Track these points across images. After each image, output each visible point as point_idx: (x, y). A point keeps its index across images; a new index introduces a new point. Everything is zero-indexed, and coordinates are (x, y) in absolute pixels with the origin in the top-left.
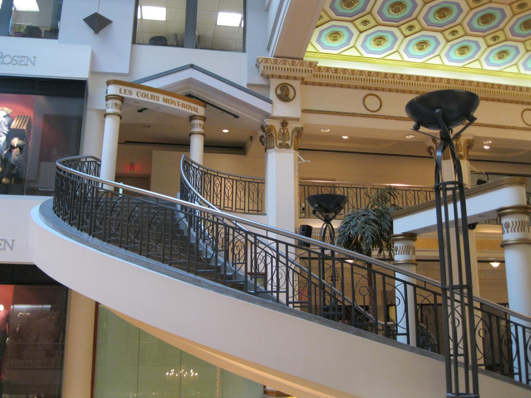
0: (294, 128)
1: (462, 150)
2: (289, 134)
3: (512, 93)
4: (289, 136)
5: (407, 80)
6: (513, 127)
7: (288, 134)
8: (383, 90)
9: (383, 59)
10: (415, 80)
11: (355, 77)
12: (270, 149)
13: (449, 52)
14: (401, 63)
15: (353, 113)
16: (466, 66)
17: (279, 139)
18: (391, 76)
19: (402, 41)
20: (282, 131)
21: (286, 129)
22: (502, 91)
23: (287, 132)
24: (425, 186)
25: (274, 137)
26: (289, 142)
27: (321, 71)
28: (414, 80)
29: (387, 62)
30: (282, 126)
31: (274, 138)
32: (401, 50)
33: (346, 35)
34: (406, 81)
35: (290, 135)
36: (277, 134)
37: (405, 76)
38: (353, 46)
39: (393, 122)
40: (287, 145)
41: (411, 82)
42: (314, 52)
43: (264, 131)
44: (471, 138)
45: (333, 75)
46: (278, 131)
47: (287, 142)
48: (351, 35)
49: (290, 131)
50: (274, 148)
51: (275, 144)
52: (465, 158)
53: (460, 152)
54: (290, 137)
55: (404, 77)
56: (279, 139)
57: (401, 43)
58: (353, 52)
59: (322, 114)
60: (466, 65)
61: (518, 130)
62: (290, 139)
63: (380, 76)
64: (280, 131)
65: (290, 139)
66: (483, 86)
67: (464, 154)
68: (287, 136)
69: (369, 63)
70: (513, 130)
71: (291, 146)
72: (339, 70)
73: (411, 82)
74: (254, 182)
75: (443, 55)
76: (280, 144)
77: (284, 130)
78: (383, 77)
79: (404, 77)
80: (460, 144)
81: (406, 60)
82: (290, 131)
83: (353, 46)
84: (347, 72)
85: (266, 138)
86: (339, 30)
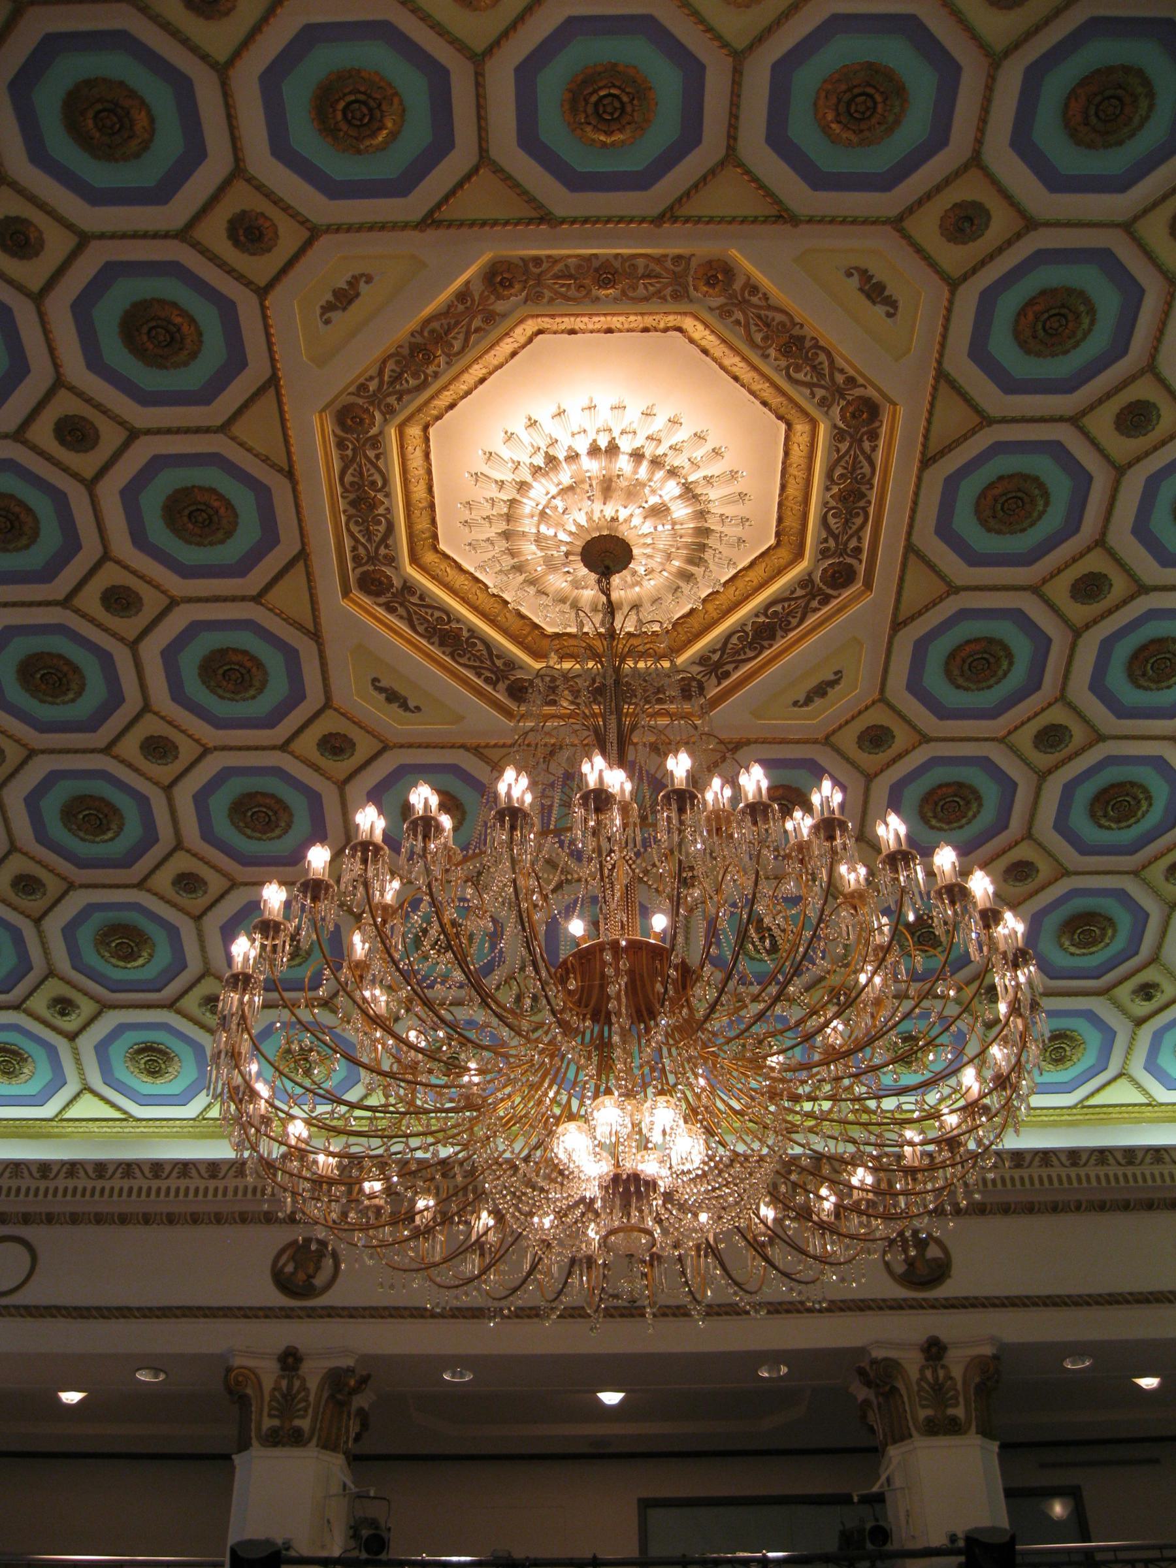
0: (325, 1371)
1: (957, 1399)
2: (307, 1396)
3: (1017, 1177)
4: (307, 1401)
5: (122, 1178)
6: (1110, 1295)
7: (949, 1382)
8: (50, 1219)
9: (1084, 1107)
10: (149, 1175)
11: (52, 1185)
12: (895, 1442)
13: (1156, 1057)
14: (117, 1128)
15: (118, 1309)
16: (1091, 1102)
17: (924, 1402)
18: (64, 1170)
19: (1133, 1038)
20: (929, 1374)
21: (943, 1367)
22: (194, 1182)
23: (304, 1388)
24: (1146, 1542)
25: (906, 1399)
26: (959, 1412)
27: (52, 1175)
28: (203, 1178)
29: (70, 1128)
30: (927, 1359)
31: (903, 1402)
32: (1137, 1069)
33: (1093, 1038)
34: (117, 1183)
35: (312, 1398)
36: (267, 1398)
37: (227, 1167)
38: (1120, 1075)
39: (61, 1325)
40: (954, 1420)
41: (135, 1184)
42: (1141, 1105)
43: (868, 1384)
44: (988, 1350)
45: (1063, 1172)
46: (913, 1373)
47: (951, 1411)
48: (1109, 1036)
49: (313, 1384)
50: (911, 1436)
51: (911, 1424)
52: (973, 1429)
53: (951, 1406)
54: (309, 1405)
55: (110, 1171)
56: (924, 1402)
57: (78, 1061)
58: (1122, 1094)
59: (42, 1316)
60: (1092, 1094)
61: (784, 1315)
62: (961, 1399)
63: (1111, 1160)
64: (923, 1378)
65: (961, 1399)
66: (1036, 1162)
67: (313, 1430)
68: (299, 1402)
69: (49, 1136)
70: (952, 1311)
71: (310, 1439)
72: (55, 1169)
73: (135, 1184)
74: (1163, 1559)
75: (1137, 1069)
76: (929, 1421)
77: (935, 1371)
78: (206, 1175)
79: (110, 1171)
80: (951, 1378)
81: (1161, 1100)
82: (313, 1384)
83: (1120, 1075)
84: (194, 1171)
85: (879, 1405)
86: (1072, 1027)
